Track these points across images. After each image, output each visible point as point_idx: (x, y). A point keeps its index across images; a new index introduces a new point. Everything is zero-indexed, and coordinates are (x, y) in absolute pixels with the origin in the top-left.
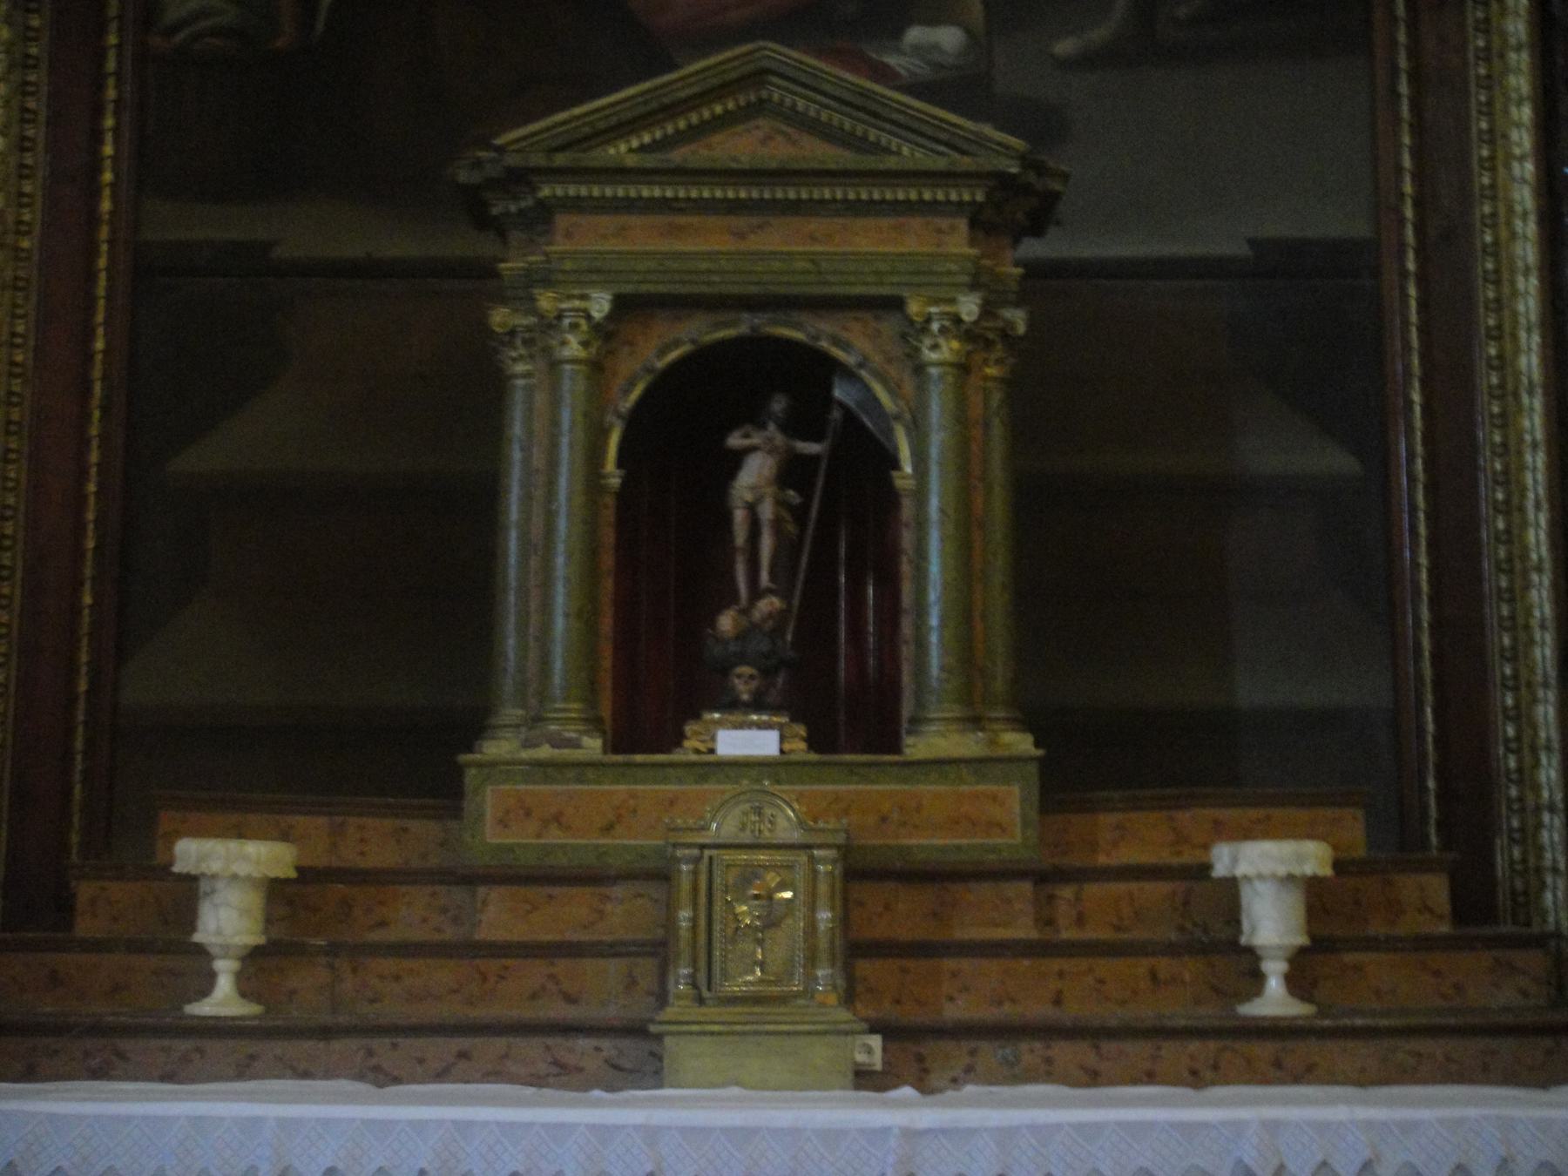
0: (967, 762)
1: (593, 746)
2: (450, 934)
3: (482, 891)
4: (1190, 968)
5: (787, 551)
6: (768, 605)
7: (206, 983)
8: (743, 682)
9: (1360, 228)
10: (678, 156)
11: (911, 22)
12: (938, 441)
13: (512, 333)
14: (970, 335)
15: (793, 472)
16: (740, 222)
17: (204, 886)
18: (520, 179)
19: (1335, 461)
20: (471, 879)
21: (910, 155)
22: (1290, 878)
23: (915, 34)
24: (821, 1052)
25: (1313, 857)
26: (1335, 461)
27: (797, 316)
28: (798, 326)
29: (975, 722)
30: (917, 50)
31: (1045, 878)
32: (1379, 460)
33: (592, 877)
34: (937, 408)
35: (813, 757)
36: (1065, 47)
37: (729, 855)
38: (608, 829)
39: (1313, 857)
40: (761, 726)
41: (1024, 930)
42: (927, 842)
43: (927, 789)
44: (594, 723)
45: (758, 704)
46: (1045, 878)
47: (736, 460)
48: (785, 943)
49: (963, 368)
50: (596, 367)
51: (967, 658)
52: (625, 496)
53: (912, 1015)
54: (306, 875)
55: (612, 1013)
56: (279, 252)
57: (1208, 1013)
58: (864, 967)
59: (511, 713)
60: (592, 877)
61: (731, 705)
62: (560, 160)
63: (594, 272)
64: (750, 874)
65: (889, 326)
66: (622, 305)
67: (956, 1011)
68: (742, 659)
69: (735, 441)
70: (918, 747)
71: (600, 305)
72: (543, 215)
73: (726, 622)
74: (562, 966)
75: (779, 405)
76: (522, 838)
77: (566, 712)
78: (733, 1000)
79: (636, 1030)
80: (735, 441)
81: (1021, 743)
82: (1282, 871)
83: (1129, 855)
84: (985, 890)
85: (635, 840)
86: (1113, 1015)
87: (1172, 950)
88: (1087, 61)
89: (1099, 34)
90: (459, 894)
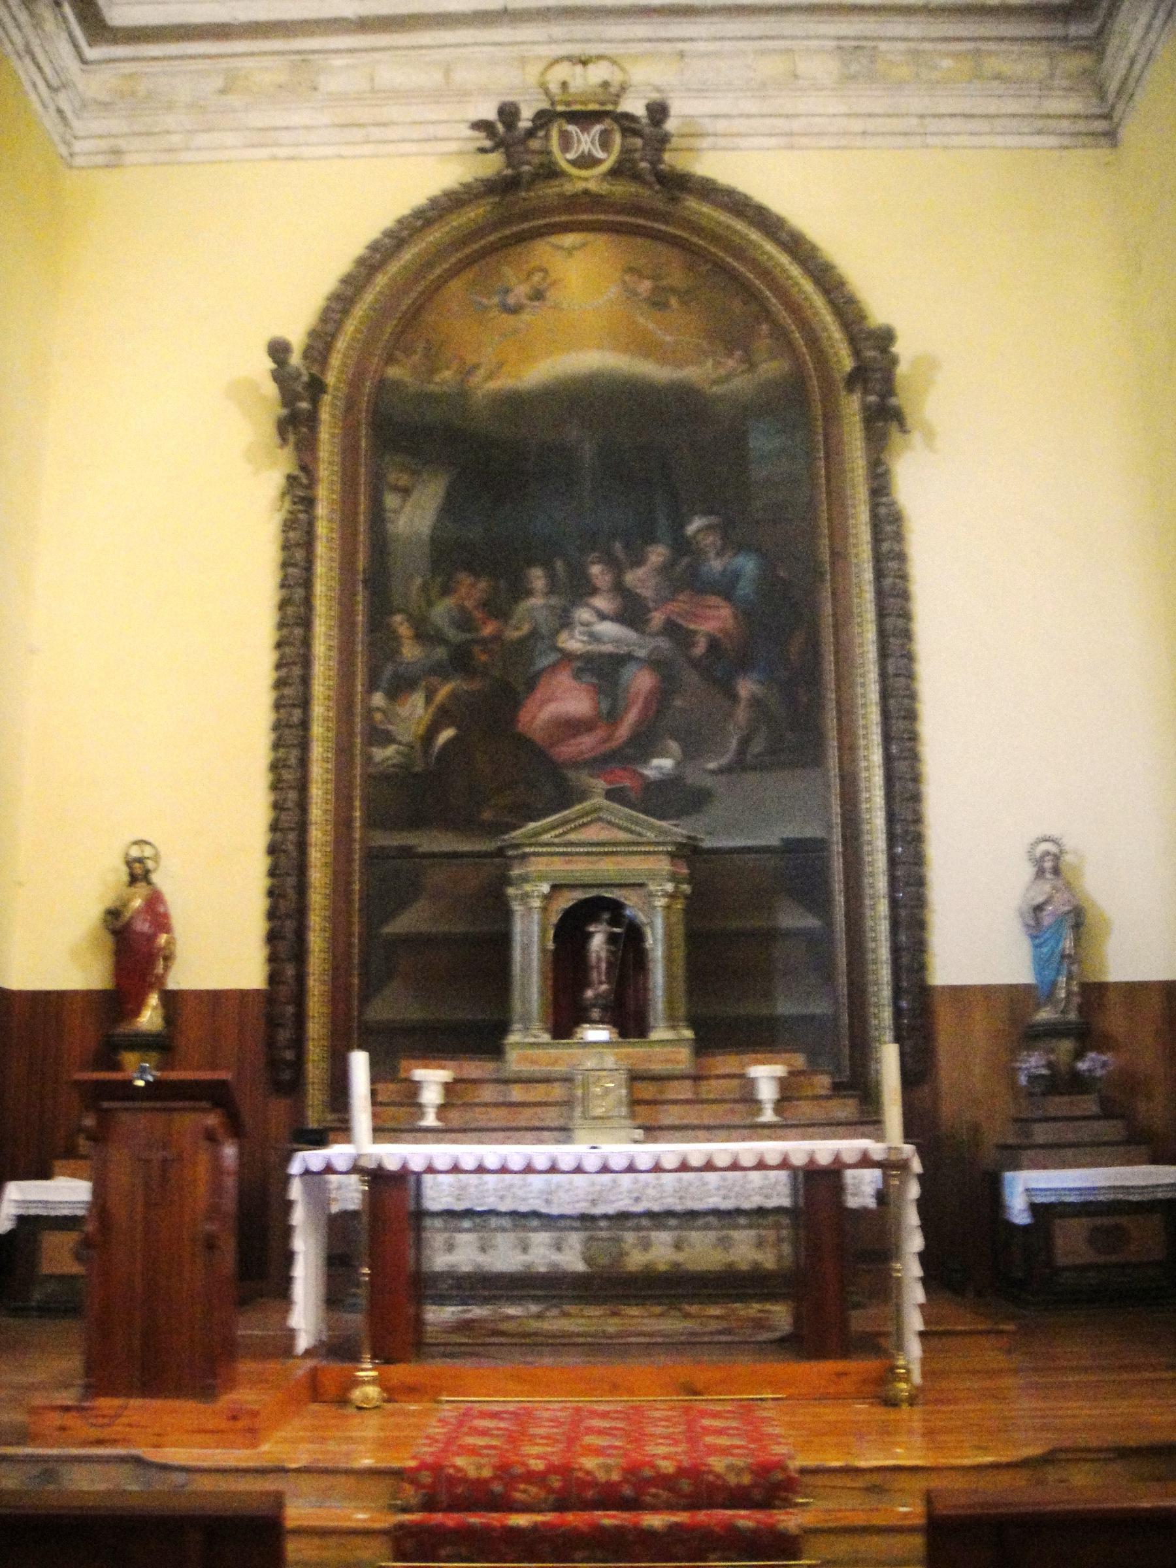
0: (668, 1041)
1: (546, 1037)
2: (501, 1099)
3: (512, 1086)
4: (739, 1107)
5: (610, 965)
6: (604, 987)
7: (422, 1116)
8: (596, 1014)
9: (820, 833)
10: (572, 837)
11: (654, 757)
12: (660, 932)
13: (516, 896)
14: (667, 895)
15: (612, 939)
16: (590, 858)
17: (425, 1085)
18: (517, 846)
19: (811, 922)
20: (507, 1082)
21: (650, 835)
22: (774, 1078)
23: (656, 762)
24: (623, 1133)
25: (779, 1070)
26: (811, 922)
27: (609, 889)
28: (612, 892)
29: (673, 1027)
30: (656, 768)
31: (697, 1078)
32: (829, 924)
33: (547, 1080)
34: (659, 922)
35: (620, 1040)
36: (712, 766)
37: (608, 1517)
38: (553, 1064)
39: (779, 1070)
40: (604, 1029)
41: (689, 1095)
42: (657, 1067)
43: (657, 1049)
44: (547, 1030)
45: (601, 1022)
46: (697, 1078)
47: (590, 935)
48: (611, 1100)
49: (668, 908)
50: (544, 909)
51: (670, 1002)
52: (556, 952)
53: (648, 1124)
54: (457, 1081)
55: (556, 1124)
56: (420, 850)
57: (748, 1122)
58: (638, 1109)
59: (517, 1026)
60: (547, 1080)
61: (592, 1021)
62: (533, 840)
63: (542, 878)
64: (599, 1078)
65: (641, 891)
66: (555, 888)
67: (667, 1121)
68: (594, 1006)
69: (592, 929)
70: (655, 1035)
71: (545, 888)
72: (524, 856)
73: (589, 993)
74: (538, 1110)
75: (606, 916)
76: (526, 1068)
77: (536, 1025)
78: (595, 1118)
79: (563, 1129)
80: (592, 929)
81: (688, 1034)
82: (771, 1075)
83: (727, 1071)
84: (676, 1083)
85: (561, 1069)
86: (712, 1122)
87: (736, 1101)
88: (720, 771)
89: (724, 760)
90: (502, 1087)
